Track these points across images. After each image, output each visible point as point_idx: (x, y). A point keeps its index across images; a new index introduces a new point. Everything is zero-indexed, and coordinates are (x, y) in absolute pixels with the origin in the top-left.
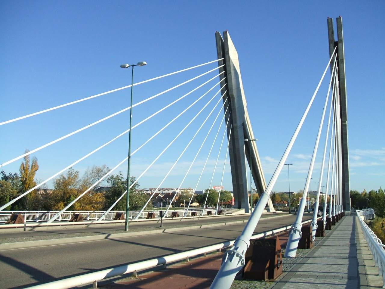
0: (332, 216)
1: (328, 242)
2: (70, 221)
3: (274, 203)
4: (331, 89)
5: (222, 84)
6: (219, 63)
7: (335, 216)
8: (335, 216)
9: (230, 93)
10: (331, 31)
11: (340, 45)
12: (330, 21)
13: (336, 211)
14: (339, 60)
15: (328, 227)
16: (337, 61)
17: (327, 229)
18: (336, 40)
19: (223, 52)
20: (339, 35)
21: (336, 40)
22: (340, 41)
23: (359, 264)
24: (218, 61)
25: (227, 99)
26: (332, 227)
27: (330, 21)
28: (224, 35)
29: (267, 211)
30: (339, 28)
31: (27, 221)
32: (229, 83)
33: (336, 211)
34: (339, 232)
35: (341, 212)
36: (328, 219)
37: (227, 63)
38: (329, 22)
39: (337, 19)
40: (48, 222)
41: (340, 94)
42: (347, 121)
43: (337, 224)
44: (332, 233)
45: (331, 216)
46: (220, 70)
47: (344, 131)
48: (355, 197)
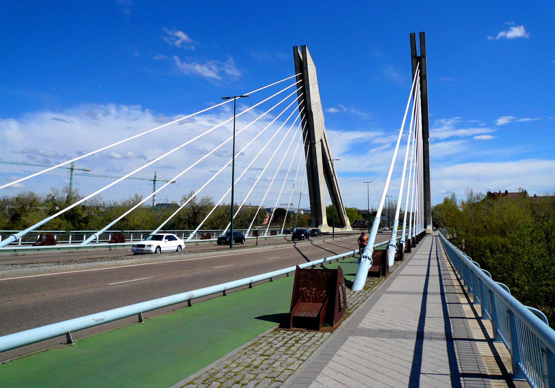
0: (411, 237)
1: (415, 257)
2: (110, 242)
3: (121, 222)
4: (413, 97)
5: (299, 101)
6: (297, 79)
7: (415, 237)
8: (415, 237)
9: (308, 109)
10: (414, 46)
11: (423, 60)
12: (412, 35)
13: (412, 233)
14: (422, 76)
15: (408, 251)
16: (419, 70)
17: (406, 252)
18: (419, 54)
19: (301, 67)
20: (423, 50)
21: (419, 54)
22: (423, 56)
23: (450, 376)
24: (296, 76)
25: (305, 115)
26: (412, 249)
27: (412, 35)
28: (302, 49)
29: (430, 224)
30: (423, 43)
31: (72, 241)
32: (307, 99)
33: (412, 233)
34: (422, 250)
35: (414, 236)
36: (407, 241)
37: (305, 78)
38: (412, 37)
39: (420, 33)
40: (82, 243)
41: (422, 113)
42: (429, 139)
43: (420, 242)
44: (417, 250)
45: (403, 239)
46: (298, 86)
47: (426, 149)
48: (424, 58)
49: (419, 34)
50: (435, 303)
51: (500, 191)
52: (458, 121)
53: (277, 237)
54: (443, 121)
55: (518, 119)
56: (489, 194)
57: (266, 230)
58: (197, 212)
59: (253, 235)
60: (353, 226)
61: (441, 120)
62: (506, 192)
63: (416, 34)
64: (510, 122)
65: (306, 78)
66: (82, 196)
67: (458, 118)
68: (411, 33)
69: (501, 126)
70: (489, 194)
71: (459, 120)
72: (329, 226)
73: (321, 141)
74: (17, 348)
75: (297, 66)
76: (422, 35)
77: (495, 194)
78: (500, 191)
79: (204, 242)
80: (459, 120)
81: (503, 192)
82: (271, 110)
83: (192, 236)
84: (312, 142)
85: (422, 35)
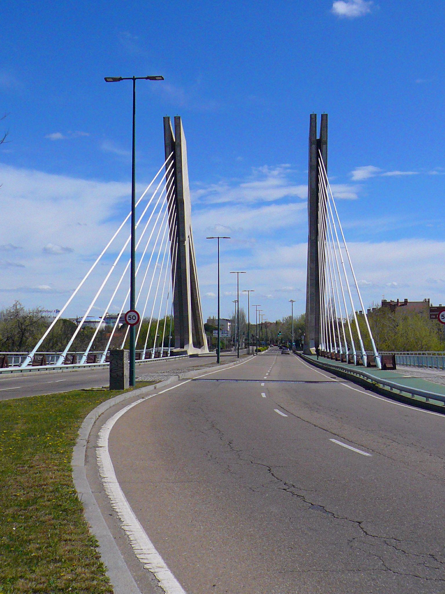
12: (313, 117)
27: (313, 117)
38: (313, 118)
49: (321, 115)
50: (148, 554)
51: (398, 299)
52: (288, 170)
53: (47, 369)
54: (265, 169)
55: (385, 172)
56: (384, 303)
57: (143, 351)
58: (25, 329)
59: (107, 360)
60: (210, 349)
61: (260, 168)
62: (406, 301)
63: (317, 117)
64: (373, 176)
65: (179, 158)
66: (117, 315)
67: (288, 165)
68: (312, 113)
69: (360, 182)
70: (384, 303)
71: (288, 168)
72: (194, 347)
73: (189, 237)
74: (309, 381)
75: (167, 142)
76: (324, 118)
77: (391, 303)
78: (398, 299)
79: (39, 370)
80: (288, 168)
81: (402, 300)
82: (141, 200)
83: (28, 360)
84: (181, 239)
85: (325, 118)
